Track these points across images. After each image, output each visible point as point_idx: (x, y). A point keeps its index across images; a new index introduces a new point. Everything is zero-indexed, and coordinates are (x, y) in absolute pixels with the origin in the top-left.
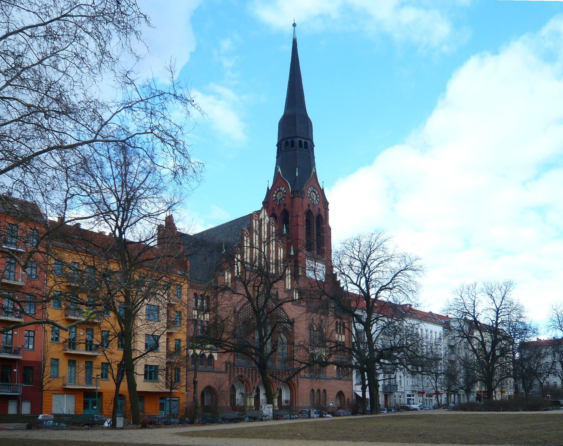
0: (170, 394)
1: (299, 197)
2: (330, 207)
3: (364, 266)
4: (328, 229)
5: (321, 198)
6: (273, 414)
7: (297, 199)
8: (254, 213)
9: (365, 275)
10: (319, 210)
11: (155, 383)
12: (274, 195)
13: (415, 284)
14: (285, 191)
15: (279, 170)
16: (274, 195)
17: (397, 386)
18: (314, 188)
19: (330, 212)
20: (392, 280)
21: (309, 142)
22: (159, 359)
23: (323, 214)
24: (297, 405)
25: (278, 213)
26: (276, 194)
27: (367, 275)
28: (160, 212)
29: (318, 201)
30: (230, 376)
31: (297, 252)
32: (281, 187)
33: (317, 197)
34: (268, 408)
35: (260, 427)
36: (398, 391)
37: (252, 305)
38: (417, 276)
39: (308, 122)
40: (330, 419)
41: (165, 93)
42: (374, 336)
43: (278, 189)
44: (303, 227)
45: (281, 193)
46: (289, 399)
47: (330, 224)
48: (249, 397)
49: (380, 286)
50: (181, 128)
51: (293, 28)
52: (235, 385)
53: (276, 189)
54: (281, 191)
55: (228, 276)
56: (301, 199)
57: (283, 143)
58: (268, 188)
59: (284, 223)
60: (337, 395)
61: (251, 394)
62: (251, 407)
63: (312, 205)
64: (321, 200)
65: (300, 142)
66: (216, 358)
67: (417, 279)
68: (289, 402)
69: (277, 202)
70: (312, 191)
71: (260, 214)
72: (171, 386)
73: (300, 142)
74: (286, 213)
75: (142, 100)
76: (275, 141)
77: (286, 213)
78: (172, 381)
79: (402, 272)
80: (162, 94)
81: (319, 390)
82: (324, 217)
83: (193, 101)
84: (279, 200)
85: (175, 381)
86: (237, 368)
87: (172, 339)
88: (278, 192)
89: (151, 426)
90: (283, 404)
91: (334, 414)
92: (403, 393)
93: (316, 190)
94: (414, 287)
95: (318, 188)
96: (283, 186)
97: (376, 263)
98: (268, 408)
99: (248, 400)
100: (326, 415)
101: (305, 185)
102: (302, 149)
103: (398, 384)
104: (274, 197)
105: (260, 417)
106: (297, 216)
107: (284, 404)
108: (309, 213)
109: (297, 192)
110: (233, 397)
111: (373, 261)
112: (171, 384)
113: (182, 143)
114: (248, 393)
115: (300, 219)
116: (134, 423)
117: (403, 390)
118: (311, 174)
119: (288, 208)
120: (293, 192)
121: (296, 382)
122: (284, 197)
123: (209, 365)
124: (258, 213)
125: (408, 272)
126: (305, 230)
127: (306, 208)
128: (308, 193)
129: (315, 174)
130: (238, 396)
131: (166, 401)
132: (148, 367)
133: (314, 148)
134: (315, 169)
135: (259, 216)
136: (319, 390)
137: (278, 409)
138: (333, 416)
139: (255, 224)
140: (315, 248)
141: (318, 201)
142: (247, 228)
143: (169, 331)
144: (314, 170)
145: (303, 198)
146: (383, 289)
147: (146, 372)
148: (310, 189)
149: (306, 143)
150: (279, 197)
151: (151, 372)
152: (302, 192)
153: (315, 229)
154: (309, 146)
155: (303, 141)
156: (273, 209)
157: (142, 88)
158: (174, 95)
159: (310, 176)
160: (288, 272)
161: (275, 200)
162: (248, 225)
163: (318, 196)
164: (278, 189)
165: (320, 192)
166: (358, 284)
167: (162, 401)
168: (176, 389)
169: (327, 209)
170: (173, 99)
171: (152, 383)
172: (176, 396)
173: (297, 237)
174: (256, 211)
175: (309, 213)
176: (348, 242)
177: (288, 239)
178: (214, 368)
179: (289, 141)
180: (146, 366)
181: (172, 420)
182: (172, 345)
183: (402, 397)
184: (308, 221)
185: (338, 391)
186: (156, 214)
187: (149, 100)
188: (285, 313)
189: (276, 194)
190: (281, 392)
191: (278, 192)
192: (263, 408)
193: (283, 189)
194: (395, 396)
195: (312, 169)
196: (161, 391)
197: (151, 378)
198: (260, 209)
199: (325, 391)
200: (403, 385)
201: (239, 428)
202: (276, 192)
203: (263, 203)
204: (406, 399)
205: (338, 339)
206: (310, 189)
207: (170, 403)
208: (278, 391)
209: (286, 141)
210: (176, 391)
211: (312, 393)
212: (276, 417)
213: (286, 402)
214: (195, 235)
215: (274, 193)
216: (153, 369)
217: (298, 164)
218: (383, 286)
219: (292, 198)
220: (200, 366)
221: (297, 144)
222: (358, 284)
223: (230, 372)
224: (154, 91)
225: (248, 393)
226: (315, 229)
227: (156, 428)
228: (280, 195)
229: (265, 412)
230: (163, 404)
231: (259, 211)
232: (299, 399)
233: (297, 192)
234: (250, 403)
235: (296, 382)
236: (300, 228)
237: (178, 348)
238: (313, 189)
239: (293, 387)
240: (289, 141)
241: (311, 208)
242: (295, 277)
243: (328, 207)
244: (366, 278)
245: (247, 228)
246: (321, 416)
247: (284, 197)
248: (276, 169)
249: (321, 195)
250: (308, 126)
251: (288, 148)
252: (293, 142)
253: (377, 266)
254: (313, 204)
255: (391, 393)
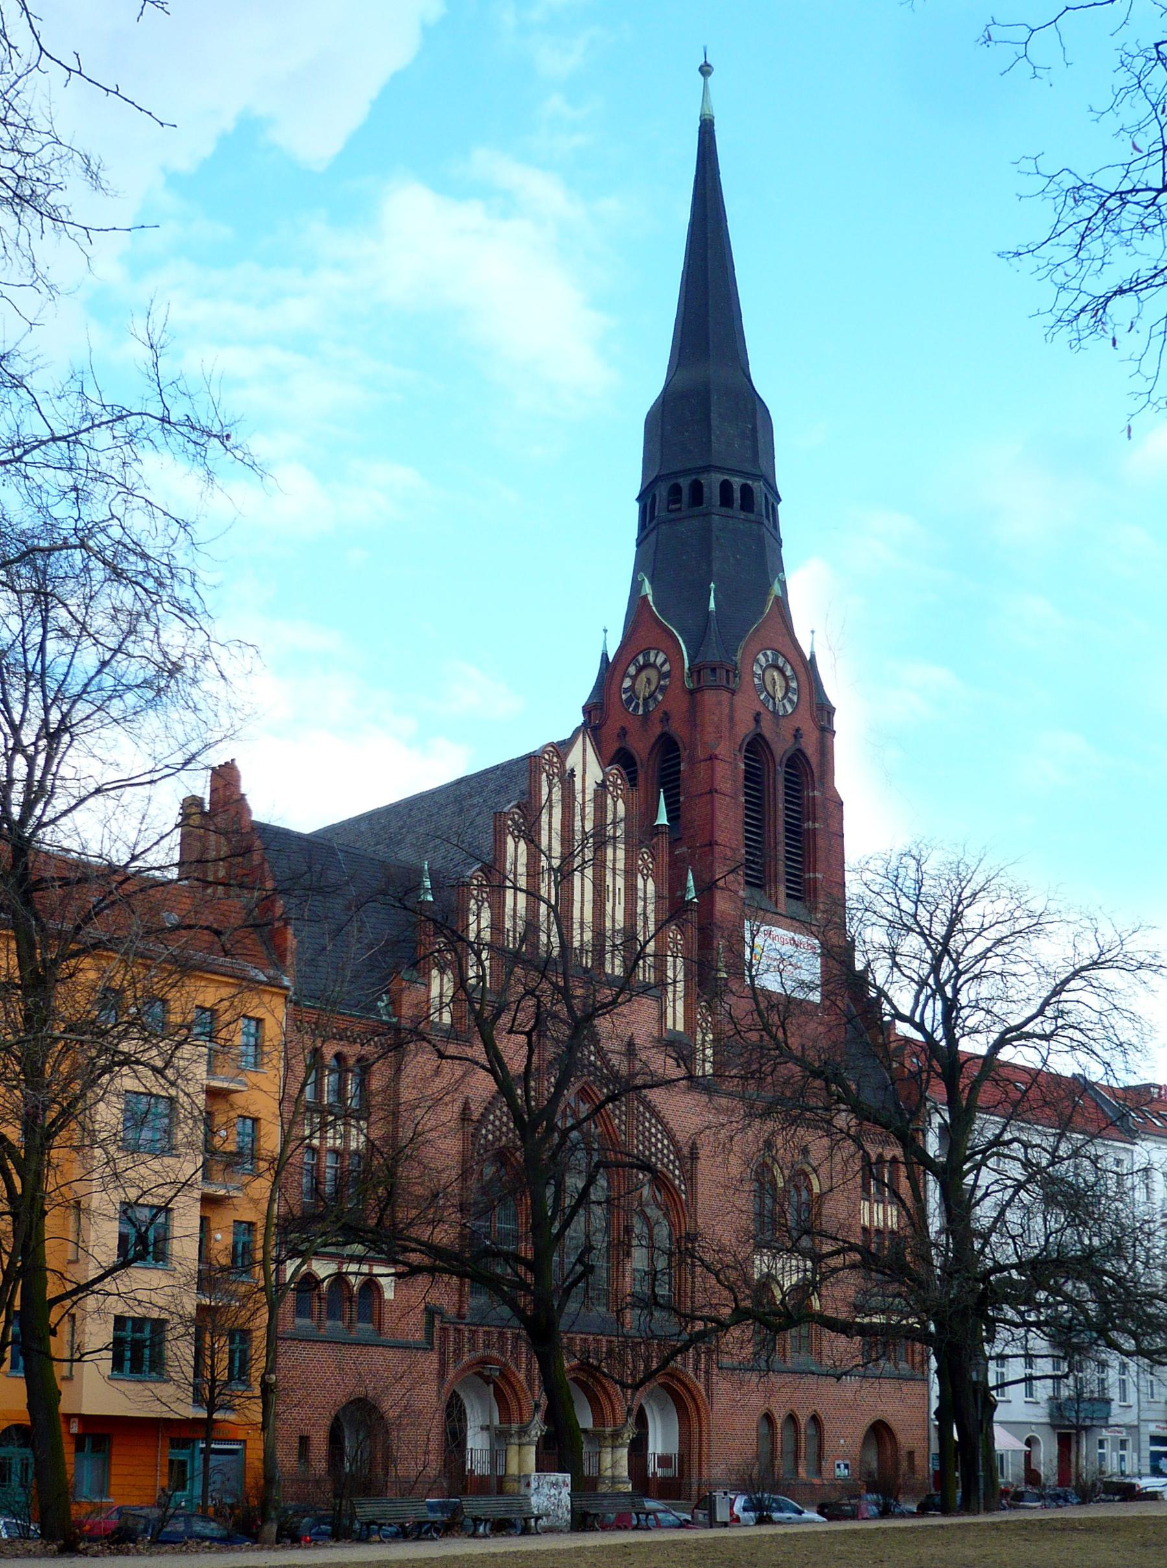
0: (207, 1425)
1: (718, 687)
2: (838, 722)
3: (942, 950)
4: (831, 806)
5: (805, 691)
6: (573, 1511)
7: (710, 698)
8: (544, 750)
9: (940, 987)
10: (797, 734)
11: (151, 1386)
12: (627, 683)
13: (1134, 1018)
14: (666, 668)
15: (647, 589)
16: (627, 683)
17: (1108, 1402)
18: (777, 652)
19: (837, 741)
20: (1046, 1003)
21: (757, 486)
22: (130, 1302)
23: (811, 751)
24: (705, 1472)
25: (640, 747)
26: (634, 678)
27: (948, 990)
28: (156, 776)
29: (790, 701)
30: (443, 1364)
31: (707, 889)
32: (652, 654)
33: (787, 689)
34: (554, 1485)
35: (494, 1555)
36: (1111, 1421)
37: (512, 1104)
38: (1140, 990)
39: (754, 411)
40: (819, 1528)
41: (132, 414)
42: (984, 1213)
43: (641, 659)
44: (734, 797)
45: (652, 674)
46: (674, 1449)
47: (836, 785)
48: (515, 1440)
49: (999, 1028)
50: (184, 525)
51: (702, 78)
52: (462, 1395)
53: (634, 659)
54: (654, 665)
55: (440, 985)
56: (725, 696)
57: (662, 491)
58: (605, 656)
59: (662, 785)
60: (866, 1438)
61: (523, 1431)
62: (614, 1479)
63: (770, 717)
64: (806, 697)
65: (726, 487)
66: (389, 1295)
67: (1140, 1003)
68: (675, 1462)
69: (637, 705)
70: (769, 666)
71: (566, 755)
72: (212, 1398)
73: (726, 487)
74: (668, 747)
75: (54, 439)
76: (632, 480)
77: (668, 747)
78: (214, 1379)
79: (1084, 974)
80: (121, 418)
81: (792, 1418)
82: (814, 760)
83: (228, 436)
84: (645, 699)
85: (231, 1377)
86: (459, 1331)
87: (223, 1221)
88: (640, 670)
89: (96, 1548)
90: (651, 1470)
91: (829, 1511)
92: (1133, 1429)
93: (787, 660)
94: (1126, 1032)
95: (791, 654)
96: (659, 650)
97: (979, 945)
98: (554, 1485)
99: (513, 1450)
100: (800, 1512)
101: (743, 644)
102: (730, 512)
103: (1114, 1393)
104: (626, 690)
105: (520, 1523)
106: (712, 758)
107: (653, 1468)
108: (756, 747)
109: (714, 670)
110: (455, 1439)
111: (970, 936)
112: (212, 1391)
113: (188, 580)
114: (515, 1427)
115: (721, 769)
116: (47, 1535)
117: (1130, 1418)
118: (764, 602)
119: (677, 728)
120: (696, 671)
121: (701, 1387)
122: (662, 689)
123: (362, 1318)
124: (561, 749)
125: (1106, 976)
126: (741, 812)
127: (745, 728)
128: (754, 674)
129: (782, 605)
130: (476, 1442)
131: (192, 1457)
132: (129, 1324)
133: (781, 508)
134: (783, 584)
135: (563, 762)
136: (792, 1418)
137: (629, 1488)
138: (830, 1518)
139: (549, 791)
140: (782, 875)
141: (790, 701)
142: (518, 806)
143: (211, 1190)
144: (776, 589)
145: (733, 692)
146: (1009, 1042)
147: (118, 1344)
148: (761, 656)
149: (746, 491)
150: (642, 690)
151: (137, 1346)
152: (732, 671)
153: (781, 806)
154: (760, 500)
155: (737, 482)
156: (623, 733)
157: (55, 401)
158: (162, 420)
159: (762, 613)
160: (675, 969)
161: (629, 701)
162: (523, 793)
163: (794, 685)
164: (641, 659)
165: (800, 669)
166: (917, 1019)
167: (182, 1455)
168: (231, 1409)
169: (826, 731)
170: (157, 436)
171: (140, 1387)
172: (230, 1436)
173: (712, 834)
174: (551, 745)
175: (756, 747)
176: (878, 865)
177: (674, 843)
178: (379, 1329)
179: (685, 483)
180: (120, 1321)
181: (198, 1527)
182: (222, 1239)
183: (1130, 1445)
184: (754, 778)
185: (868, 1421)
186: (147, 778)
187: (83, 437)
188: (660, 1120)
189: (634, 678)
190: (642, 1422)
191: (640, 670)
192: (534, 1485)
193: (659, 660)
194: (1101, 1444)
195: (770, 585)
196: (178, 1417)
197: (136, 1368)
198: (567, 735)
199: (815, 1419)
200: (1132, 1398)
201: (415, 1560)
202: (632, 670)
203: (587, 710)
204: (1146, 1454)
205: (886, 1224)
206: (761, 656)
207: (206, 1461)
208: (631, 1420)
209: (672, 482)
210: (231, 1417)
211: (765, 1430)
212: (582, 1521)
213: (664, 1461)
214: (316, 835)
215: (625, 674)
216: (147, 1333)
217: (716, 566)
218: (1010, 1030)
219: (691, 692)
220: (328, 1324)
221: (713, 493)
222: (917, 1019)
223: (444, 1341)
224: (94, 409)
225: (515, 1427)
226: (781, 806)
227: (112, 1554)
228: (649, 681)
229: (538, 1502)
230: (183, 1464)
231: (563, 743)
232: (714, 1449)
233: (714, 670)
234: (520, 1467)
235: (701, 1387)
236: (721, 802)
237: (241, 1257)
238: (775, 659)
239: (690, 1405)
240: (685, 483)
241: (767, 730)
242: (700, 984)
243: (830, 721)
244: (944, 998)
245: (518, 806)
246: (761, 1521)
247: (662, 689)
248: (636, 586)
249: (803, 678)
250: (754, 430)
251: (680, 509)
252: (697, 488)
253: (983, 956)
254: (775, 713)
255: (1081, 1429)
